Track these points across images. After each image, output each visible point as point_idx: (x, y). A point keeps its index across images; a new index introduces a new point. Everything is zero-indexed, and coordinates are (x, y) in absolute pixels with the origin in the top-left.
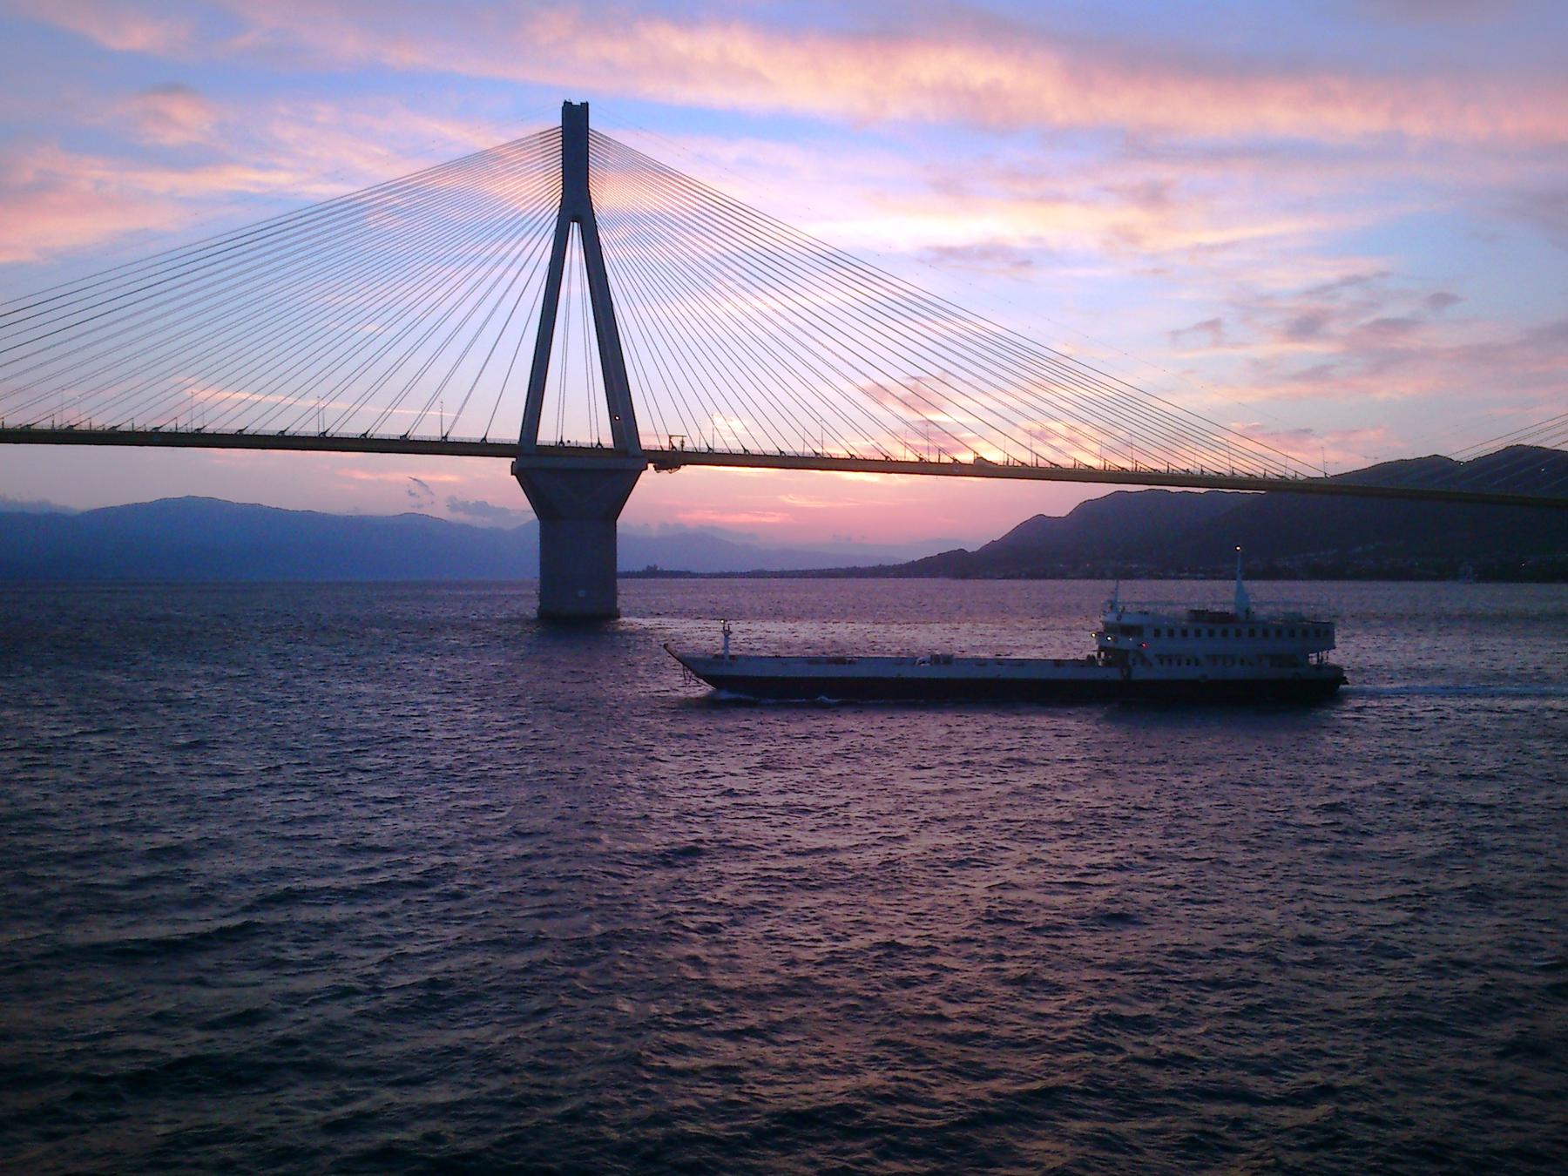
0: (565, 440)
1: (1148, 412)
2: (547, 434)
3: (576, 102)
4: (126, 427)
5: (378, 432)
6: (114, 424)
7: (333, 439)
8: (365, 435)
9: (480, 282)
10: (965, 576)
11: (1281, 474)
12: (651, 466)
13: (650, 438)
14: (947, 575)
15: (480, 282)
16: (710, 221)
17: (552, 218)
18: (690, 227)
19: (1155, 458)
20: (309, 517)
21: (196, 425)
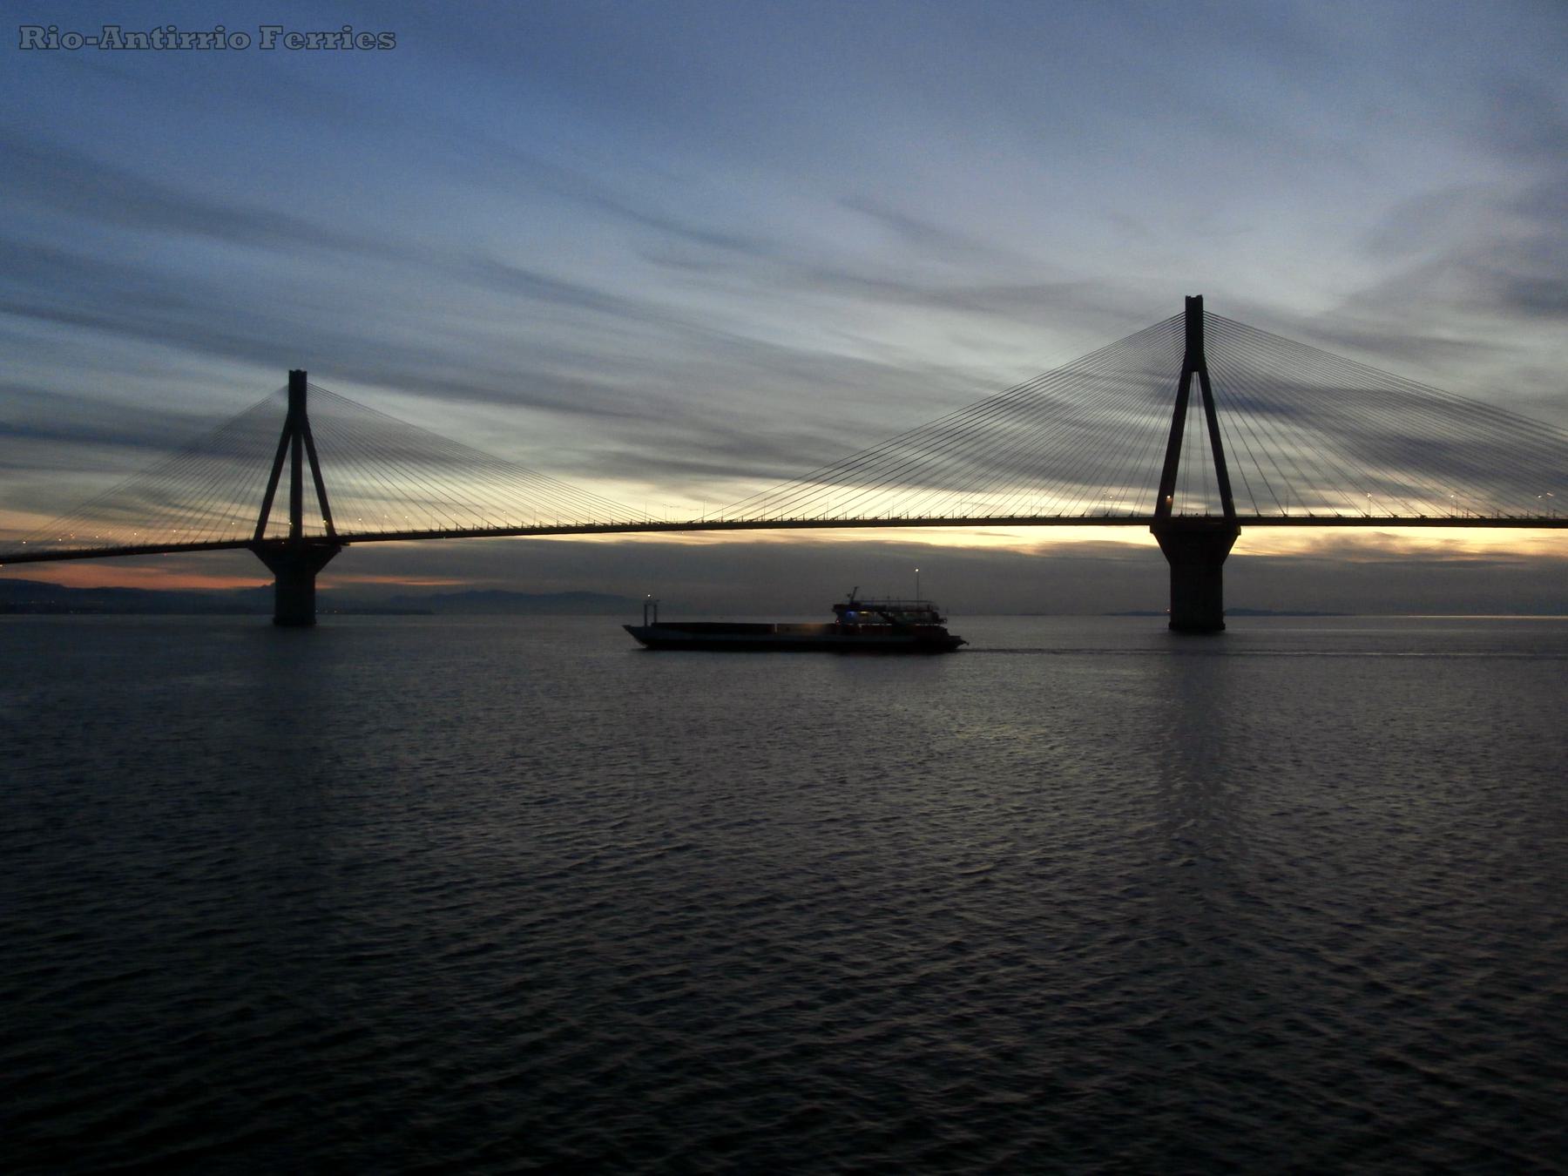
2: (267, 535)
3: (1194, 296)
17: (491, 493)
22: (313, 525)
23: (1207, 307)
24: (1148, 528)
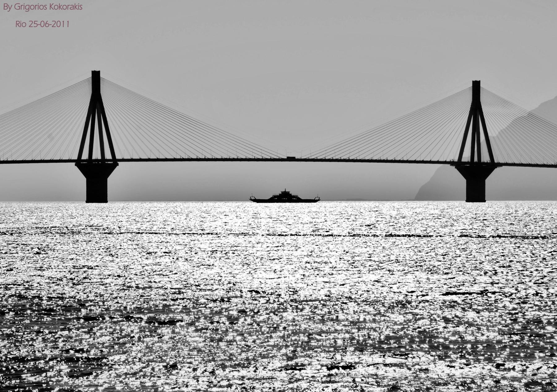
13: (75, 157)
22: (486, 158)
24: (74, 163)
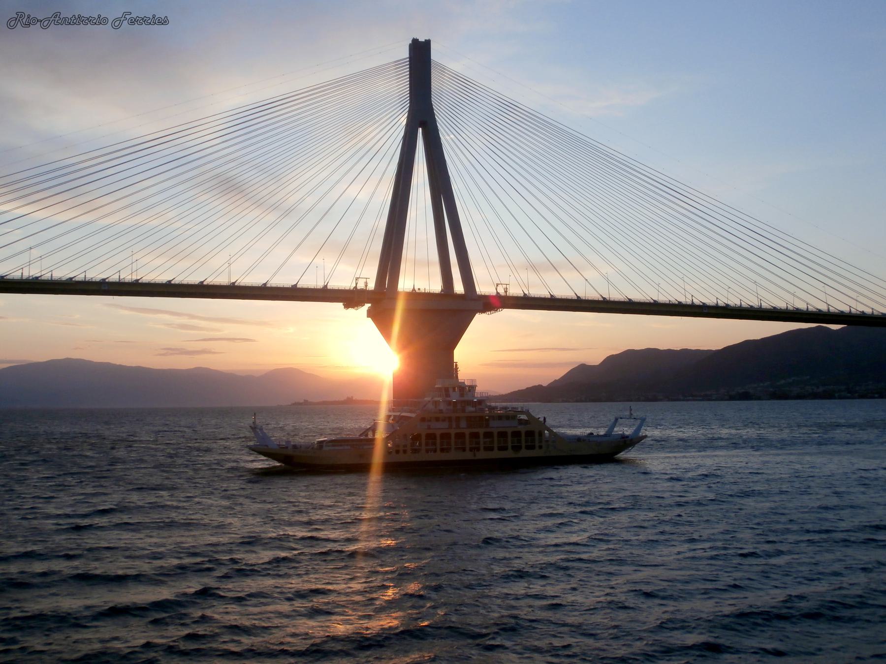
0: (416, 288)
1: (568, 168)
4: (115, 278)
5: (243, 281)
6: (71, 275)
7: (272, 289)
8: (265, 284)
9: (361, 148)
10: (550, 402)
11: (774, 306)
12: (368, 305)
13: (368, 278)
14: (540, 401)
15: (361, 148)
16: (460, 89)
18: (526, 163)
19: (780, 298)
20: (216, 371)
21: (134, 278)
23: (435, 56)
